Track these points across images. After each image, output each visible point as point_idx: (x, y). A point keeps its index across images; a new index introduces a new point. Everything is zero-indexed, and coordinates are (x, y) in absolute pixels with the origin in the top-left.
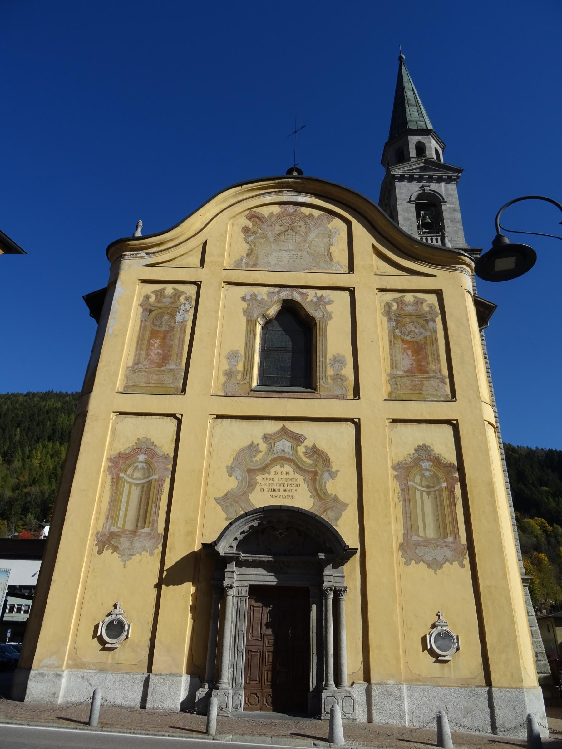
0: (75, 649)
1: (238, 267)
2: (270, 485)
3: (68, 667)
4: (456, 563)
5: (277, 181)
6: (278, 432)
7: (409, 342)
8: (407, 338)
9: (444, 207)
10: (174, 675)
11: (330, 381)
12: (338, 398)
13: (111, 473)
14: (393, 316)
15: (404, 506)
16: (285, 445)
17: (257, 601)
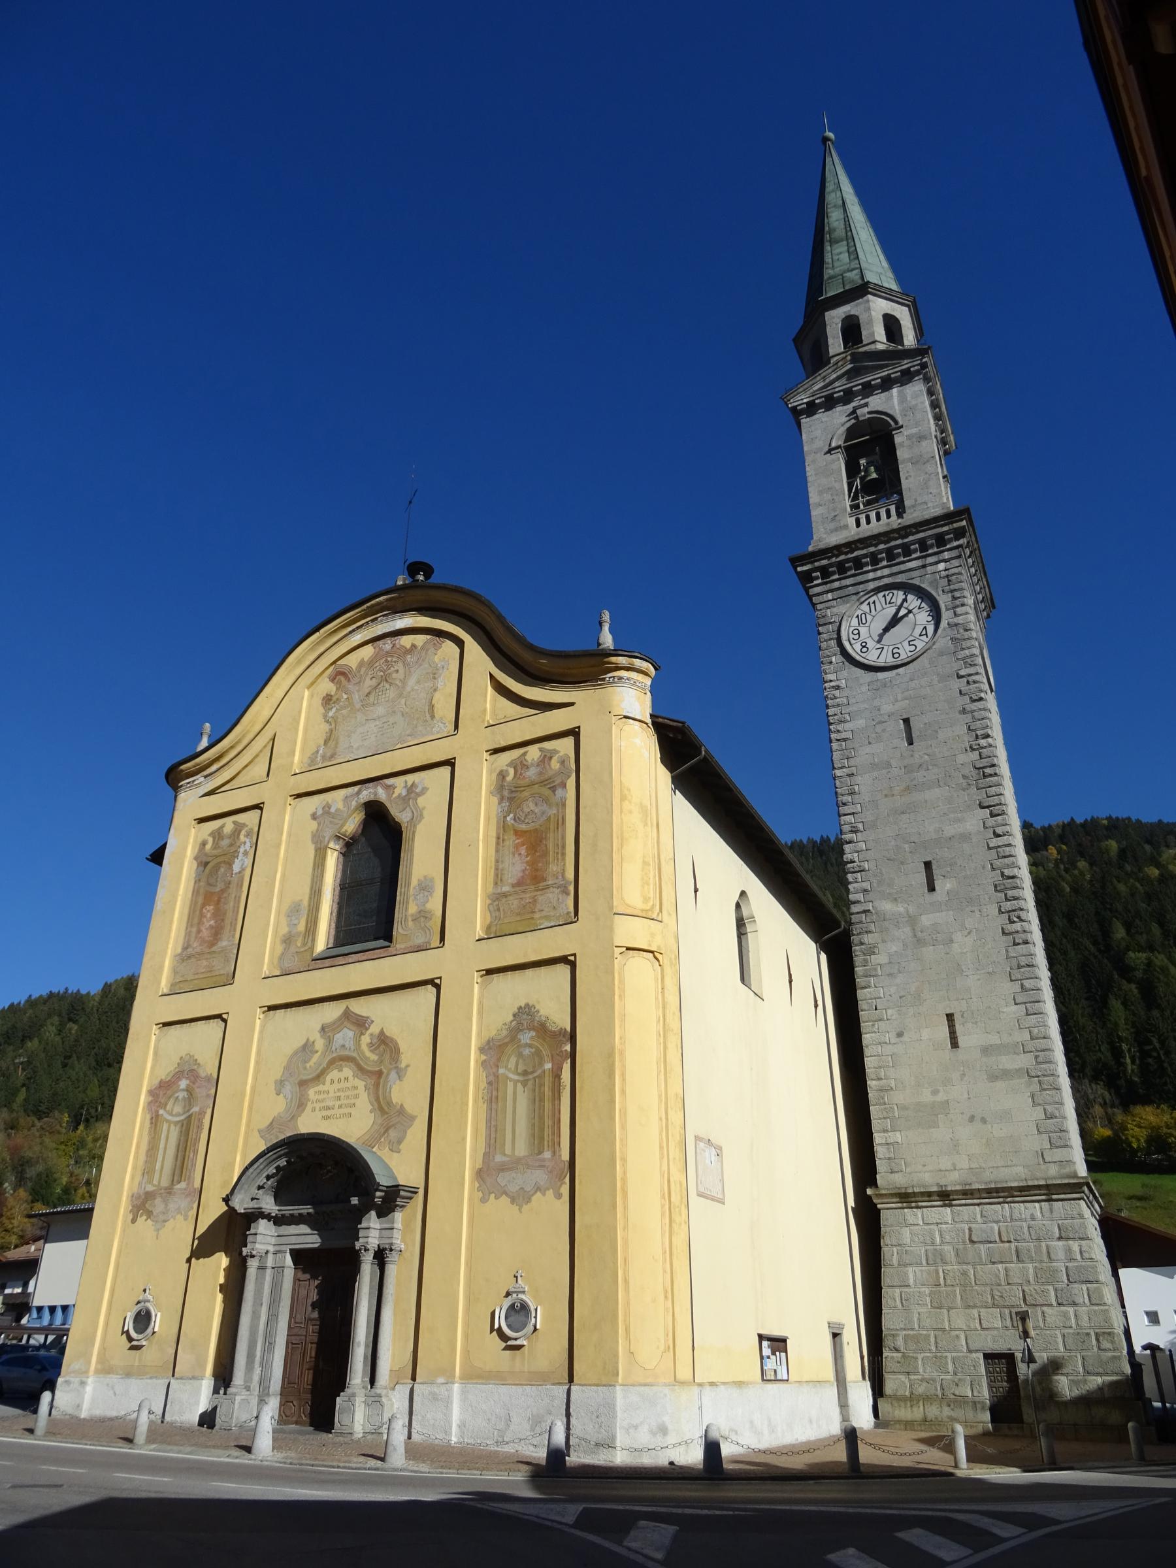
0: (103, 1349)
1: (312, 766)
2: (323, 1101)
3: (97, 1372)
4: (550, 1193)
5: (365, 607)
6: (340, 1019)
7: (526, 832)
8: (523, 827)
9: (898, 439)
10: (194, 1378)
11: (410, 923)
12: (420, 949)
13: (150, 1110)
14: (506, 793)
15: (490, 1109)
16: (346, 1036)
17: (304, 1272)
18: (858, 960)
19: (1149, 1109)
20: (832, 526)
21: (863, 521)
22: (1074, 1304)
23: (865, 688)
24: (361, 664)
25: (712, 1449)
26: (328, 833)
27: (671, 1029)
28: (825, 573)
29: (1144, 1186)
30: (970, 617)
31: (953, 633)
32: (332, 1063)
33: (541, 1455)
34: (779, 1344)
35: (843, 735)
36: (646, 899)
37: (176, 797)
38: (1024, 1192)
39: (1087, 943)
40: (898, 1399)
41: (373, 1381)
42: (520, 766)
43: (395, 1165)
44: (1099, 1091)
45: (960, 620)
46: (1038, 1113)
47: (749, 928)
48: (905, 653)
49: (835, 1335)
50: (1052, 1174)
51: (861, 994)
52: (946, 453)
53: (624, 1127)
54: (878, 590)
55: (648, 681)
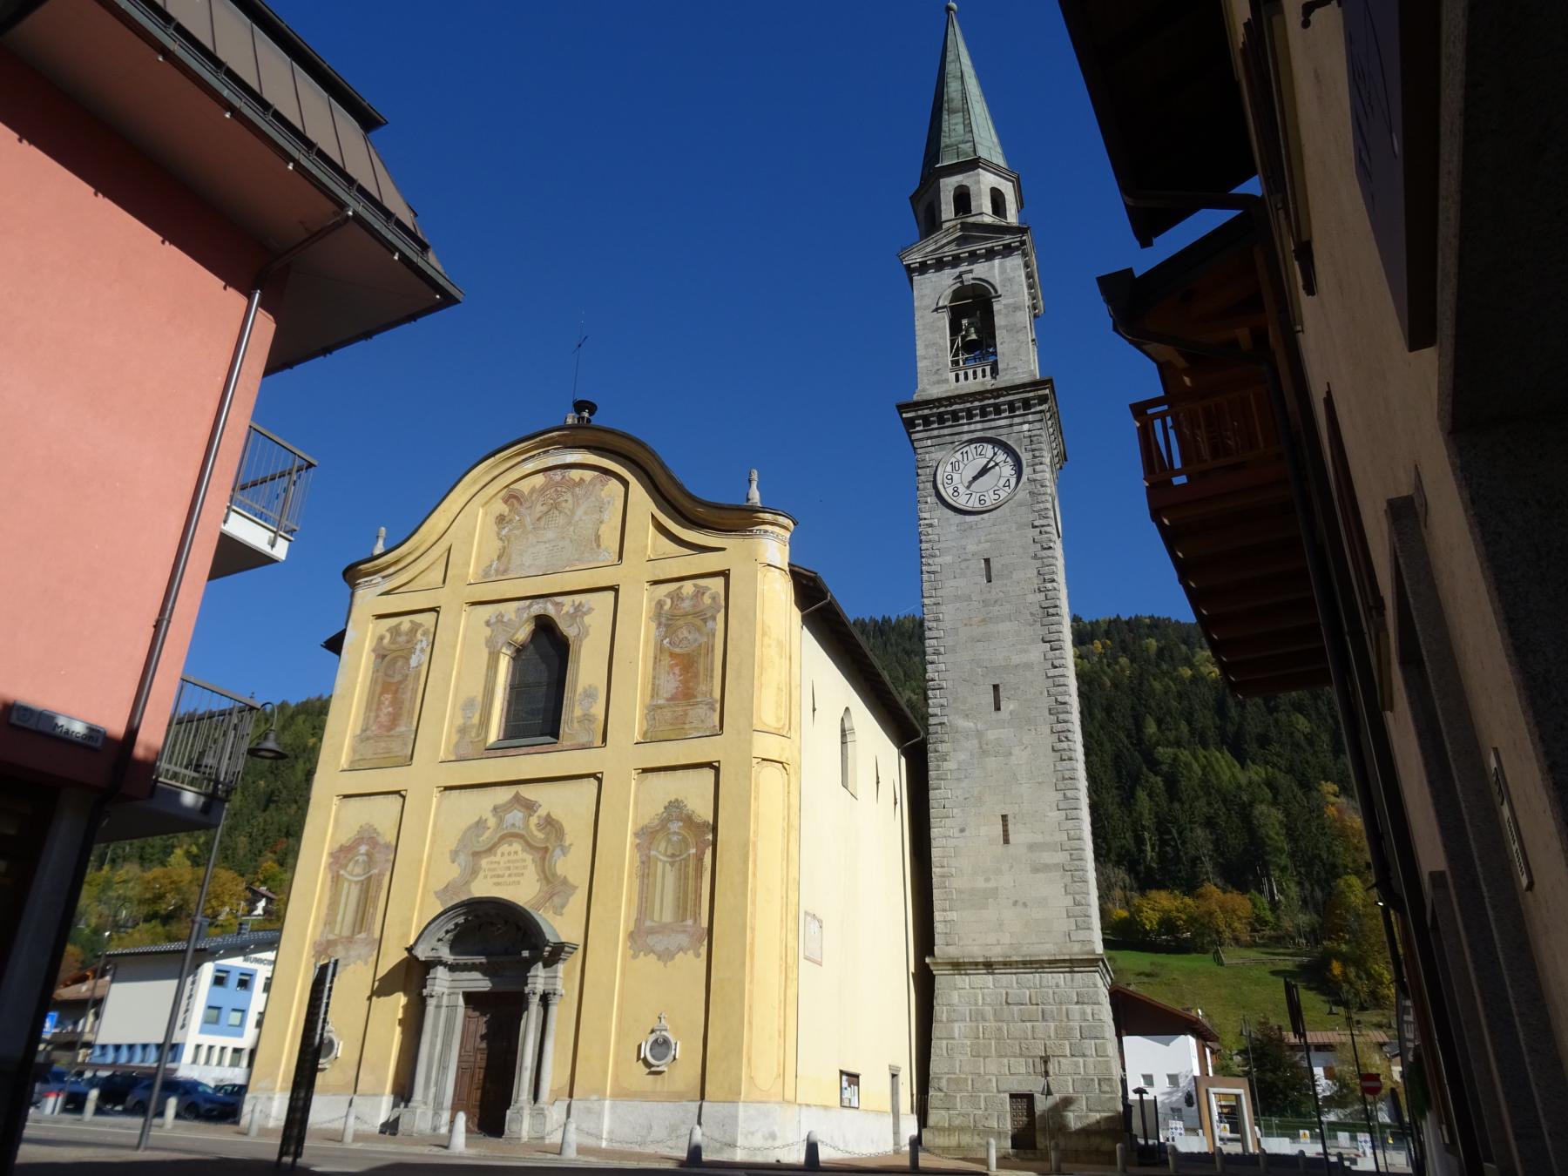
8: (678, 650)
9: (996, 307)
10: (375, 1095)
11: (576, 725)
14: (663, 620)
16: (516, 816)
18: (932, 765)
19: (1163, 893)
20: (935, 378)
21: (962, 377)
22: (1084, 1055)
23: (954, 528)
24: (533, 490)
25: (812, 1148)
26: (501, 639)
27: (792, 829)
28: (926, 421)
29: (1152, 964)
30: (1047, 475)
31: (1031, 487)
32: (502, 838)
33: (683, 1155)
34: (854, 1078)
35: (933, 568)
36: (779, 719)
37: (352, 595)
38: (1053, 964)
39: (1122, 736)
40: (939, 1129)
41: (536, 1097)
42: (676, 597)
43: (559, 926)
44: (1120, 875)
45: (1038, 477)
46: (1069, 901)
47: (849, 738)
48: (990, 500)
49: (894, 1076)
50: (1076, 951)
51: (932, 794)
52: (1035, 316)
53: (754, 903)
54: (971, 442)
55: (788, 535)
